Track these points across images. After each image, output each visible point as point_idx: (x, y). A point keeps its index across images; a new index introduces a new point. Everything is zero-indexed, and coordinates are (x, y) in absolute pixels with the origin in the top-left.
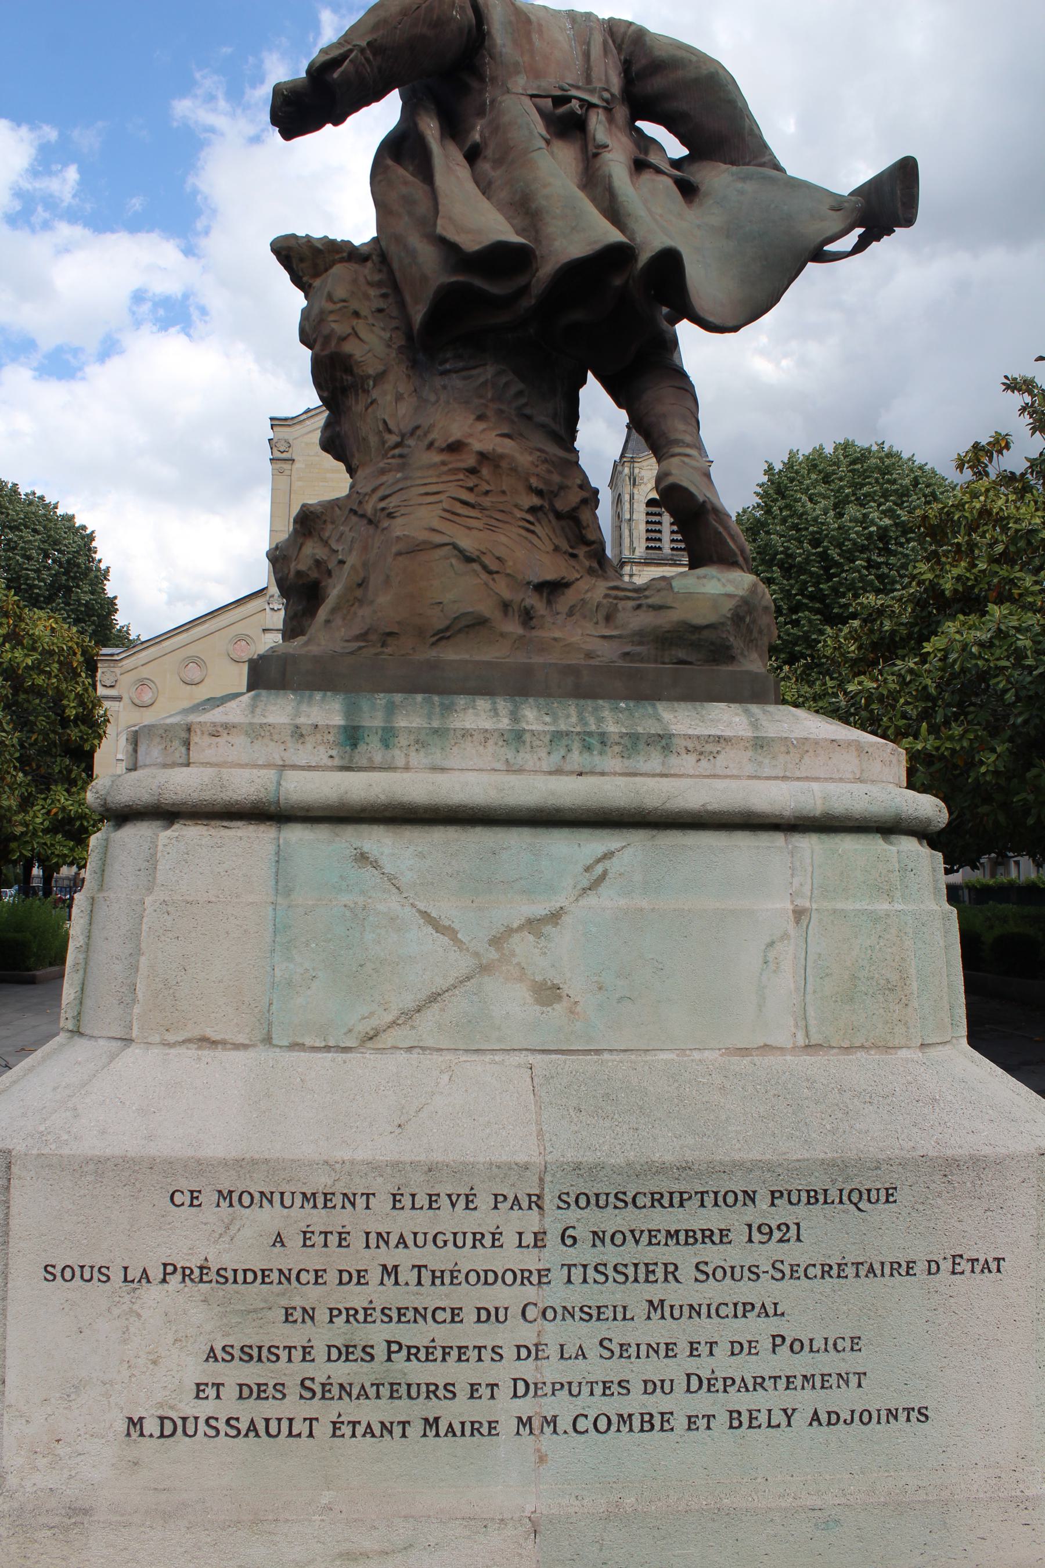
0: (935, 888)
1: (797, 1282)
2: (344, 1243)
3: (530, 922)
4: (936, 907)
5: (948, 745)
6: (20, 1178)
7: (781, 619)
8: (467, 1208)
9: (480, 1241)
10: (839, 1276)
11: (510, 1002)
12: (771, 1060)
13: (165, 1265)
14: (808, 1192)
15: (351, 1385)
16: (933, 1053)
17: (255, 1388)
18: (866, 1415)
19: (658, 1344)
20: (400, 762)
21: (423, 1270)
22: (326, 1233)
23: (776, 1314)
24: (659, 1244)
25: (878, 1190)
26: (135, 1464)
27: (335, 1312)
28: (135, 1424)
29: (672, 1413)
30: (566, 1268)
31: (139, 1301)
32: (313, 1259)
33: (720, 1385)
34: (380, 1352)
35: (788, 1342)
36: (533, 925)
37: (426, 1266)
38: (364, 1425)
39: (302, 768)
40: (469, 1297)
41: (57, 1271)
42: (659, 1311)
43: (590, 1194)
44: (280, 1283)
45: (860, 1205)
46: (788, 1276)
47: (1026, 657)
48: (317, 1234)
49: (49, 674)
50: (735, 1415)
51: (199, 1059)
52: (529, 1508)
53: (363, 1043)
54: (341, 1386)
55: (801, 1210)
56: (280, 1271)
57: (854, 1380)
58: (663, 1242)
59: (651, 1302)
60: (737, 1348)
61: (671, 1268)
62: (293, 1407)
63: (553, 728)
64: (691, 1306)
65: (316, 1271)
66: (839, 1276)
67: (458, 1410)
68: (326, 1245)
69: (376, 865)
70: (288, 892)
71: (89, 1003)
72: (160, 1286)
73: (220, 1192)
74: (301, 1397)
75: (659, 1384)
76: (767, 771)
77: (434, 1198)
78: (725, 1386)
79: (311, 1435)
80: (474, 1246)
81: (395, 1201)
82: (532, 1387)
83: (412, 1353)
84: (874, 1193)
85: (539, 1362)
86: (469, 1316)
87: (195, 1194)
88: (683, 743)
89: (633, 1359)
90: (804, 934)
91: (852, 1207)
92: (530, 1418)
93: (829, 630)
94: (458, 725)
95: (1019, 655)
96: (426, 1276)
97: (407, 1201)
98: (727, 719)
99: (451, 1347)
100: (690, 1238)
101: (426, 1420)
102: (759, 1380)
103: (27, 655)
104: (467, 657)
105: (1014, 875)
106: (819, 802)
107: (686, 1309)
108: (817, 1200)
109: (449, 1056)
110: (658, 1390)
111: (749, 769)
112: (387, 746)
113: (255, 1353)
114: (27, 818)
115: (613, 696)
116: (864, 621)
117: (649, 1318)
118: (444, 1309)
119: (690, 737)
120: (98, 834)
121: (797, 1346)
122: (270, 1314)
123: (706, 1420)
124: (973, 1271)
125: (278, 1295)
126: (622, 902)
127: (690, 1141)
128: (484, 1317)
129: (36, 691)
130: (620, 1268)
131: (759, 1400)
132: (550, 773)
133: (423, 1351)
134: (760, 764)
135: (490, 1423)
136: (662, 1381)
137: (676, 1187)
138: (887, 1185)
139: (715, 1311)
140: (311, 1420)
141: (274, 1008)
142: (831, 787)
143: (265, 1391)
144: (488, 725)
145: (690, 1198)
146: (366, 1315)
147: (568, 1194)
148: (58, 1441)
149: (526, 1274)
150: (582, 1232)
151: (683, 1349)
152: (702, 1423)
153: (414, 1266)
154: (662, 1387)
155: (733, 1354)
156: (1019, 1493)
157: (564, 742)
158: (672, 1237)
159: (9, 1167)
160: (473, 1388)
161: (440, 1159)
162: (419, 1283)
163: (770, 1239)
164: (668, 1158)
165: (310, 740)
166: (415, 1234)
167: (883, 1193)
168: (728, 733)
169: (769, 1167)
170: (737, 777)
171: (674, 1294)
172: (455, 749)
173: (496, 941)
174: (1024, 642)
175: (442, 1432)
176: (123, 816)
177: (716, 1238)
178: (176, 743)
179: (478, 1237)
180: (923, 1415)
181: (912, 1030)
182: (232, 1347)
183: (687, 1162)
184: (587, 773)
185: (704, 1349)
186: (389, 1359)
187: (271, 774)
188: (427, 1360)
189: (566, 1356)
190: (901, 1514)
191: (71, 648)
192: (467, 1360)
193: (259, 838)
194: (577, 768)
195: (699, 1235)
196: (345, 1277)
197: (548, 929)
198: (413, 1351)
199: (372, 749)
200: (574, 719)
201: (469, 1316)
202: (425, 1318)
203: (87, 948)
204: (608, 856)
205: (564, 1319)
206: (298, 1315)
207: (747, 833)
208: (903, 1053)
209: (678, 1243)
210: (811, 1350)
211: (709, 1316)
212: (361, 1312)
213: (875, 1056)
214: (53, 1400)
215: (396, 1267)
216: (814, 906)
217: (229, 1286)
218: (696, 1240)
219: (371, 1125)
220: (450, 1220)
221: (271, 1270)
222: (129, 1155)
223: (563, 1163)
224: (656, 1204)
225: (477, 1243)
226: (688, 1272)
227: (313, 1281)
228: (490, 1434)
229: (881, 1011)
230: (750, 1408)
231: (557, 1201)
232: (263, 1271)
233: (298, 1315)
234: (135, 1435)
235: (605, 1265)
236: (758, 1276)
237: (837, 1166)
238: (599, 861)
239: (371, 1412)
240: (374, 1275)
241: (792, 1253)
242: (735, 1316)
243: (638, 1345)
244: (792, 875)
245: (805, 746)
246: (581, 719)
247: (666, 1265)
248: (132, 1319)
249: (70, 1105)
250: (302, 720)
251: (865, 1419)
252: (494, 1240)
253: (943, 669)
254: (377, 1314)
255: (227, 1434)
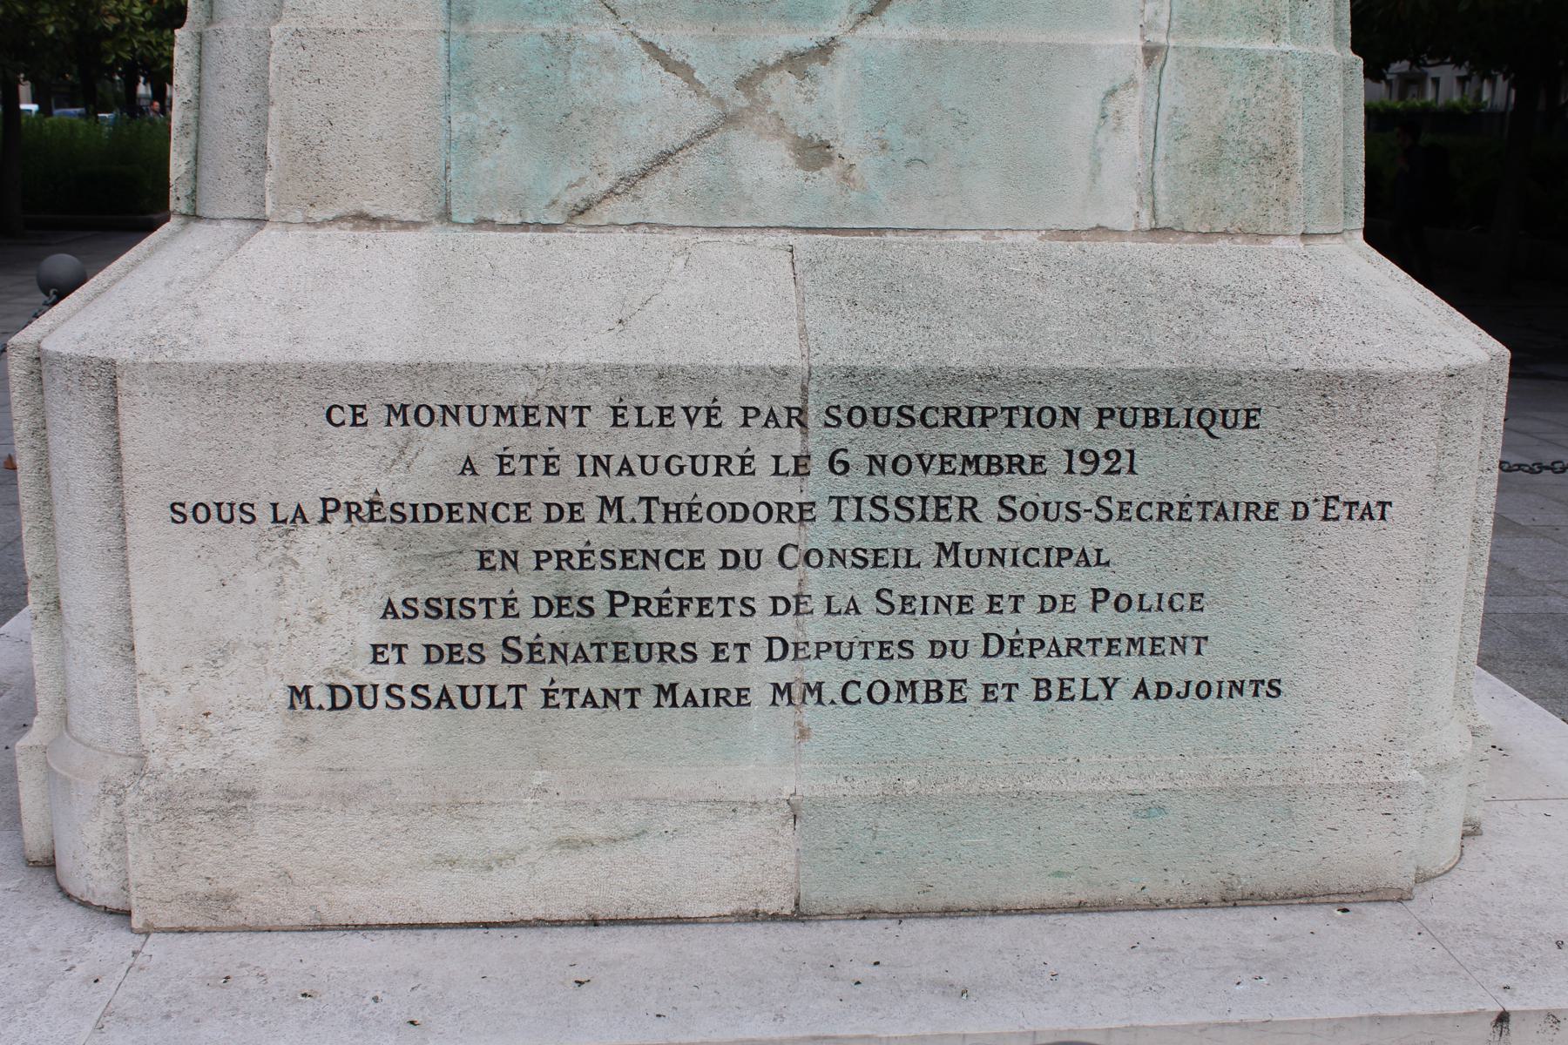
0: (1336, 30)
1: (1127, 524)
2: (552, 470)
3: (790, 57)
4: (1334, 53)
6: (129, 394)
8: (709, 424)
9: (726, 466)
10: (1180, 518)
11: (765, 164)
13: (325, 500)
14: (1147, 411)
15: (565, 645)
16: (1320, 246)
17: (446, 650)
18: (1204, 687)
19: (950, 597)
21: (654, 503)
22: (529, 458)
23: (1098, 563)
24: (953, 472)
25: (1236, 411)
26: (304, 740)
27: (543, 557)
28: (300, 694)
29: (965, 681)
30: (835, 501)
31: (295, 546)
32: (513, 489)
33: (1025, 648)
34: (601, 604)
35: (1112, 598)
36: (795, 61)
37: (657, 499)
38: (583, 693)
40: (712, 537)
41: (188, 511)
42: (952, 557)
43: (866, 408)
44: (472, 520)
45: (1212, 430)
46: (1116, 517)
48: (517, 458)
50: (1043, 684)
51: (356, 242)
52: (788, 790)
54: (554, 646)
55: (1137, 434)
56: (472, 505)
57: (1192, 646)
58: (959, 469)
59: (942, 546)
60: (1048, 604)
61: (968, 503)
62: (493, 671)
64: (993, 551)
65: (518, 505)
66: (1180, 518)
67: (697, 676)
68: (529, 472)
71: (206, 175)
72: (320, 526)
73: (390, 407)
74: (504, 660)
75: (949, 645)
77: (666, 412)
78: (1032, 649)
79: (518, 705)
80: (718, 473)
81: (616, 415)
82: (791, 648)
83: (641, 606)
84: (1231, 414)
85: (800, 618)
87: (359, 410)
89: (918, 615)
90: (1156, 81)
91: (1202, 432)
92: (788, 685)
96: (658, 511)
97: (631, 416)
99: (690, 599)
101: (660, 687)
102: (1074, 643)
107: (986, 554)
108: (1158, 422)
109: (684, 236)
110: (949, 653)
113: (444, 607)
114: (122, 7)
117: (939, 565)
118: (681, 552)
121: (1123, 603)
123: (1006, 690)
124: (1350, 517)
125: (470, 535)
126: (914, 32)
127: (997, 343)
128: (731, 562)
130: (904, 502)
131: (1074, 667)
133: (655, 604)
135: (739, 690)
136: (954, 643)
137: (978, 401)
138: (1249, 406)
139: (1022, 558)
140: (517, 687)
143: (458, 653)
145: (995, 415)
146: (582, 560)
147: (838, 407)
148: (207, 714)
149: (785, 508)
150: (855, 457)
153: (641, 499)
154: (954, 650)
155: (1043, 611)
156: (1382, 779)
158: (970, 464)
159: (114, 383)
160: (719, 648)
161: (674, 362)
162: (649, 519)
163: (1095, 470)
164: (968, 363)
166: (643, 458)
167: (1242, 415)
171: (971, 536)
173: (746, 83)
175: (680, 702)
177: (1027, 467)
179: (724, 461)
180: (1275, 689)
181: (1292, 213)
182: (415, 600)
183: (992, 369)
185: (1007, 605)
186: (613, 614)
188: (660, 614)
189: (834, 610)
190: (1239, 801)
192: (711, 615)
195: (1005, 463)
196: (555, 513)
197: (815, 67)
198: (643, 603)
202: (656, 563)
205: (832, 565)
206: (496, 560)
208: (1279, 243)
209: (978, 472)
210: (1141, 609)
211: (1015, 564)
212: (576, 556)
213: (1241, 244)
214: (195, 668)
215: (619, 500)
217: (409, 526)
218: (1001, 468)
219: (583, 321)
220: (686, 439)
221: (460, 505)
222: (269, 361)
223: (832, 369)
224: (951, 422)
225: (722, 469)
226: (988, 508)
227: (514, 518)
228: (739, 703)
229: (1254, 186)
230: (1062, 676)
231: (824, 416)
232: (450, 506)
233: (496, 560)
235: (885, 498)
236: (1079, 516)
237: (1187, 379)
240: (592, 510)
241: (1123, 488)
242: (1048, 564)
243: (925, 598)
247: (962, 499)
248: (286, 568)
251: (1203, 692)
252: (743, 465)
254: (597, 558)
255: (413, 705)
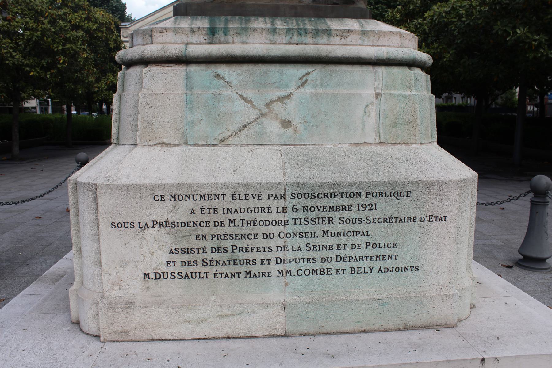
5: (432, 51)
7: (372, 7)
8: (259, 199)
11: (273, 127)
12: (367, 148)
13: (153, 221)
16: (425, 146)
17: (187, 262)
20: (231, 41)
28: (146, 275)
33: (348, 259)
34: (230, 249)
35: (371, 245)
36: (281, 99)
38: (225, 274)
39: (195, 44)
40: (260, 230)
47: (463, 17)
49: (103, 32)
52: (282, 300)
53: (220, 143)
55: (377, 199)
56: (194, 222)
57: (394, 257)
59: (324, 231)
60: (353, 247)
61: (331, 219)
63: (287, 27)
64: (338, 232)
65: (206, 222)
67: (256, 269)
68: (209, 213)
69: (223, 78)
70: (191, 89)
71: (121, 133)
76: (366, 43)
79: (207, 277)
80: (262, 212)
82: (283, 260)
83: (241, 249)
84: (402, 193)
86: (260, 236)
88: (335, 32)
91: (395, 198)
92: (282, 271)
93: (389, 10)
94: (252, 26)
95: (460, 16)
97: (237, 197)
98: (352, 24)
100: (338, 209)
101: (246, 272)
103: (94, 25)
104: (255, 2)
105: (454, 102)
106: (385, 54)
107: (336, 234)
109: (251, 147)
111: (360, 42)
112: (226, 35)
113: (186, 250)
115: (309, 16)
116: (403, 6)
119: (338, 30)
120: (121, 72)
121: (374, 246)
122: (191, 237)
127: (338, 175)
128: (265, 237)
129: (98, 38)
130: (313, 219)
131: (361, 264)
132: (286, 44)
133: (244, 249)
134: (364, 40)
136: (328, 258)
137: (333, 191)
139: (346, 234)
141: (188, 131)
142: (391, 49)
144: (263, 26)
146: (224, 237)
150: (299, 207)
151: (335, 247)
152: (341, 272)
157: (291, 32)
159: (96, 190)
162: (243, 225)
164: (330, 181)
165: (197, 33)
166: (241, 208)
167: (406, 193)
168: (352, 29)
169: (365, 184)
170: (355, 45)
171: (332, 228)
172: (251, 35)
173: (267, 105)
174: (462, 11)
175: (252, 276)
176: (130, 64)
177: (347, 209)
178: (147, 36)
180: (417, 269)
184: (300, 44)
185: (342, 247)
186: (233, 252)
187: (183, 46)
188: (246, 252)
191: (110, 22)
193: (179, 71)
194: (296, 42)
195: (341, 208)
196: (217, 224)
197: (286, 101)
198: (241, 249)
199: (220, 36)
200: (295, 24)
201: (260, 236)
202: (245, 237)
203: (119, 113)
204: (308, 74)
206: (200, 237)
207: (359, 66)
208: (414, 146)
211: (344, 236)
212: (223, 236)
213: (404, 146)
215: (234, 220)
216: (383, 92)
217: (176, 228)
219: (224, 171)
220: (252, 203)
226: (336, 221)
233: (200, 237)
234: (147, 279)
237: (390, 184)
238: (304, 76)
239: (227, 269)
240: (227, 223)
241: (374, 214)
242: (353, 236)
244: (375, 81)
245: (381, 34)
246: (297, 24)
247: (329, 218)
249: (116, 167)
250: (194, 26)
251: (397, 270)
252: (268, 210)
253: (431, 23)
254: (228, 236)
